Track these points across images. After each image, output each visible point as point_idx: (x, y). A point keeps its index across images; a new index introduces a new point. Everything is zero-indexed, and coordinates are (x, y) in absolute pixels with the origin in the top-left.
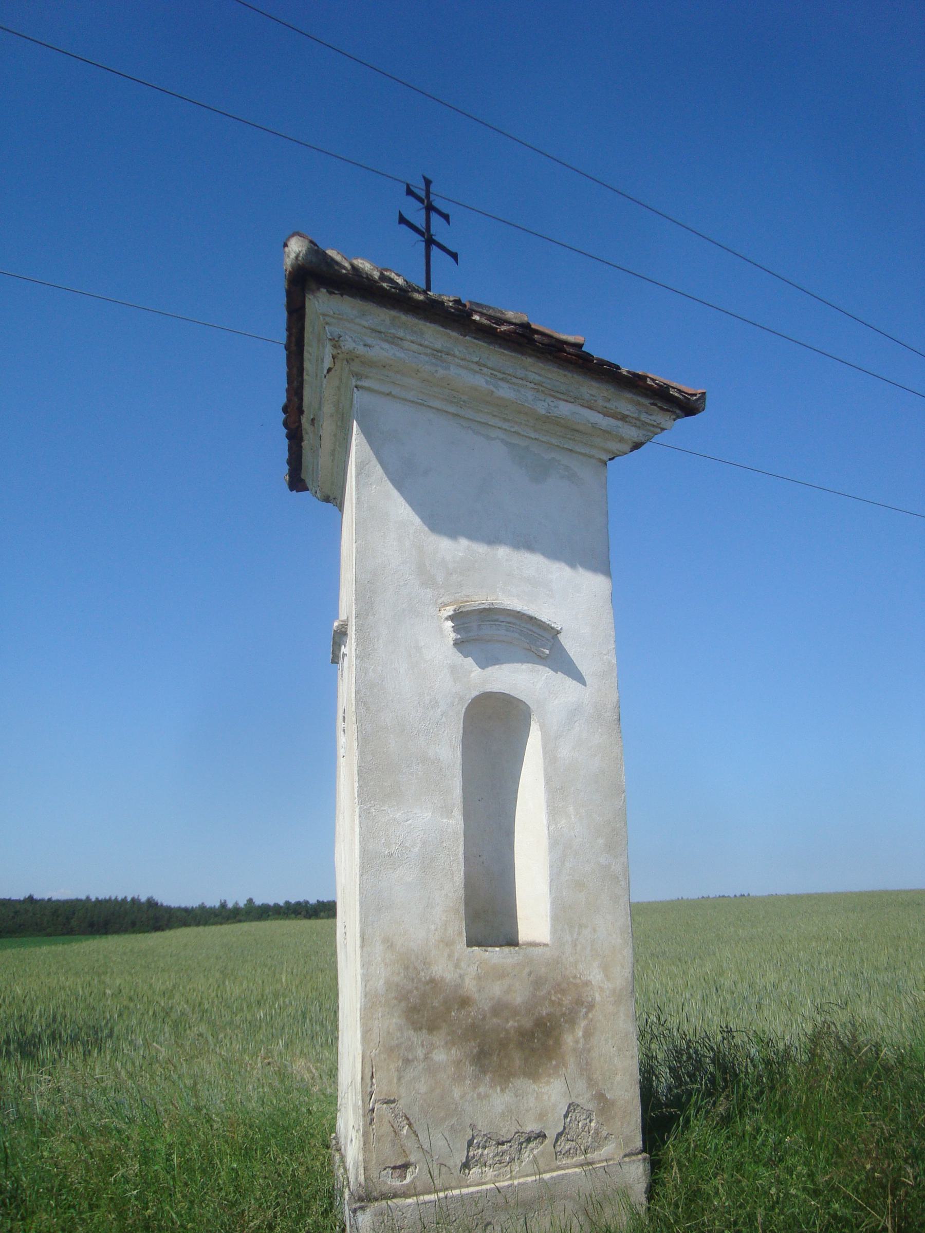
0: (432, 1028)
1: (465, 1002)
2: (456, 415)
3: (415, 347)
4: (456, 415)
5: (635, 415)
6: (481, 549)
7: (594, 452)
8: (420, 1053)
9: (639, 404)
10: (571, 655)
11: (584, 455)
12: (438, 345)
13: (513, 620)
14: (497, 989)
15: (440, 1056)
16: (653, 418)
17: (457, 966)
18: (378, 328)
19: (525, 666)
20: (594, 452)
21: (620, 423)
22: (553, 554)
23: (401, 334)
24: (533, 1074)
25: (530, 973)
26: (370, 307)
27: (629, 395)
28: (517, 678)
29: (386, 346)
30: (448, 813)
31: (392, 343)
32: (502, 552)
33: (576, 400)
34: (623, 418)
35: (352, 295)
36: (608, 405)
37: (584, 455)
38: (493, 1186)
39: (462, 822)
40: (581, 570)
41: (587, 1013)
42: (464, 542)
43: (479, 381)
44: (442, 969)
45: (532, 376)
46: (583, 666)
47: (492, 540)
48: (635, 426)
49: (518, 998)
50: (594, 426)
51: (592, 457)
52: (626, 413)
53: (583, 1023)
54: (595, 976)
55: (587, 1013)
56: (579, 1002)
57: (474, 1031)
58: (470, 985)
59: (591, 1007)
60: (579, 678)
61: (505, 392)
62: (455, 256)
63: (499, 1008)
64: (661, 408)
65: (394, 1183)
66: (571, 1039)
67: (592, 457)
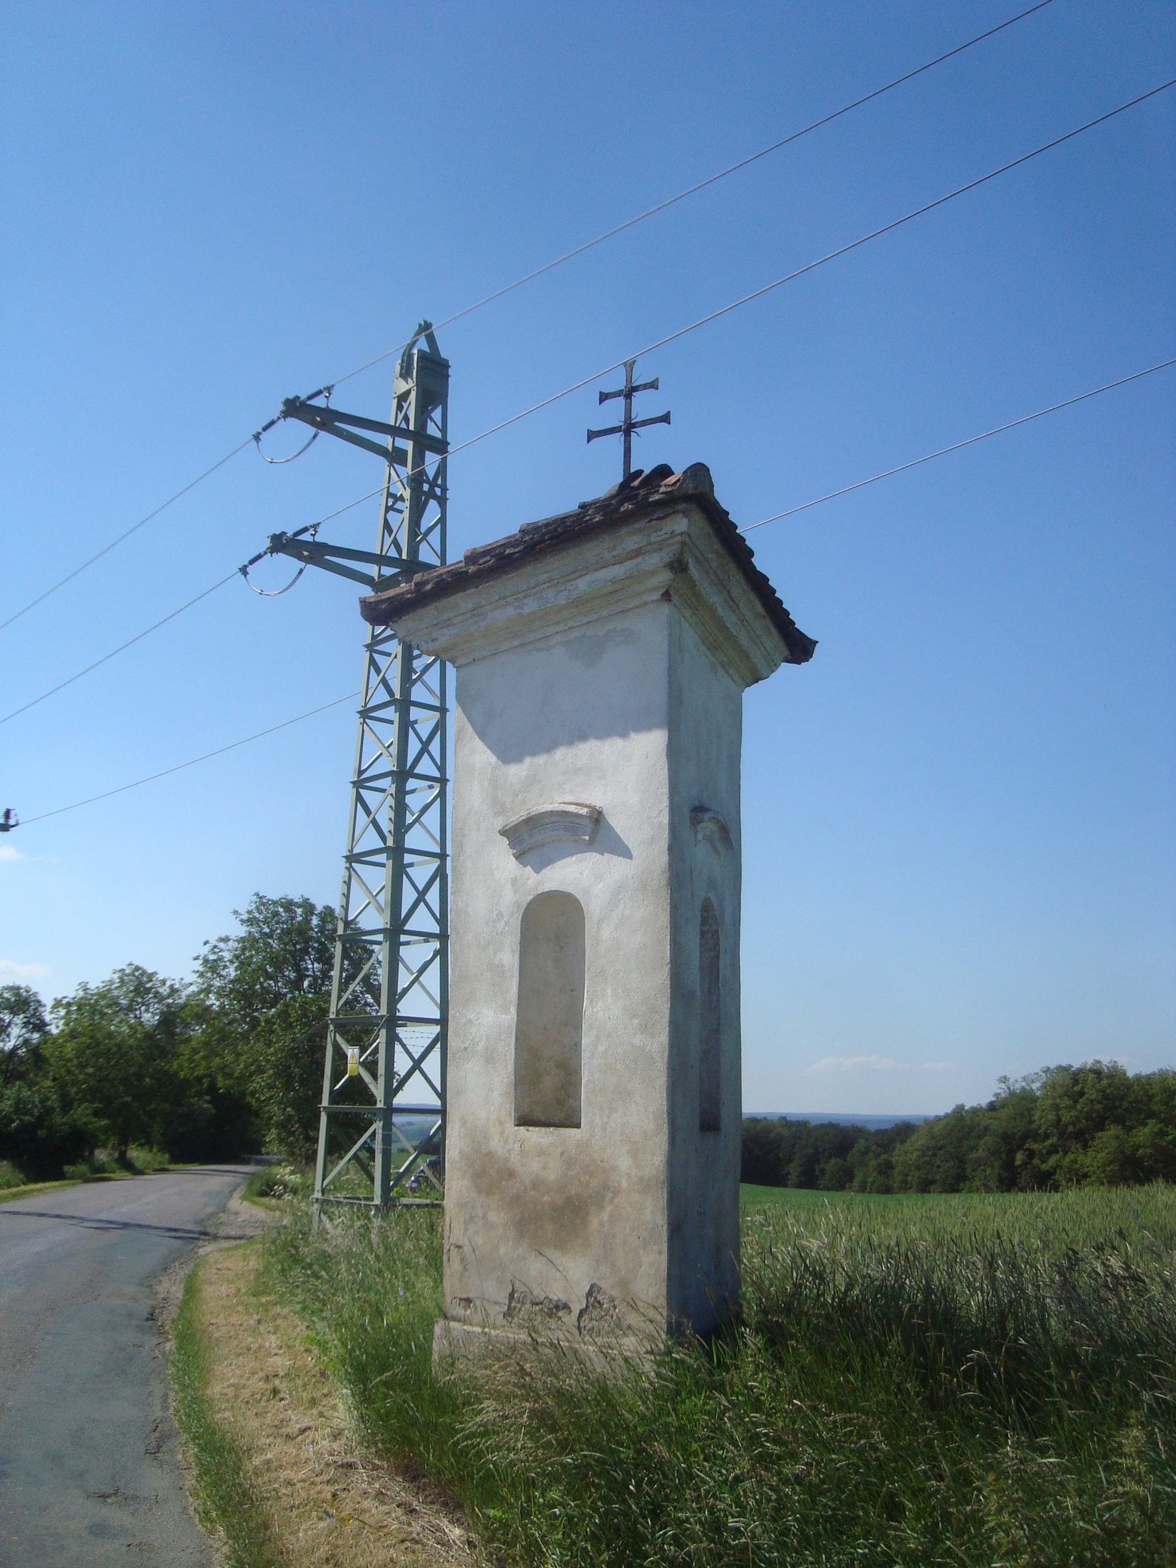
0: (489, 1193)
1: (512, 1174)
2: (522, 645)
3: (460, 618)
4: (522, 645)
5: (644, 543)
6: (541, 760)
7: (645, 598)
8: (480, 1212)
9: (640, 530)
10: (618, 831)
11: (636, 607)
12: (470, 606)
13: (554, 819)
14: (535, 1166)
15: (493, 1217)
16: (664, 531)
17: (506, 1142)
18: (435, 622)
19: (574, 858)
20: (645, 598)
21: (639, 560)
22: (603, 734)
23: (446, 616)
24: (561, 1245)
25: (562, 1154)
26: (421, 612)
27: (630, 528)
28: (573, 873)
29: (445, 631)
30: (506, 1010)
31: (447, 626)
32: (560, 753)
33: (587, 570)
34: (638, 553)
35: (407, 613)
36: (615, 553)
37: (636, 607)
38: (478, 1329)
39: (515, 1017)
40: (633, 735)
41: (613, 1198)
42: (528, 760)
43: (510, 611)
44: (495, 1144)
45: (542, 578)
46: (631, 840)
47: (549, 749)
48: (655, 551)
49: (552, 1174)
50: (614, 581)
51: (646, 603)
52: (636, 546)
53: (609, 1208)
54: (624, 1163)
55: (613, 1198)
56: (606, 1187)
57: (516, 1200)
58: (515, 1160)
59: (616, 1192)
60: (626, 853)
61: (531, 606)
62: (666, 419)
63: (537, 1183)
64: (659, 519)
65: (460, 1311)
66: (597, 1221)
67: (646, 603)
